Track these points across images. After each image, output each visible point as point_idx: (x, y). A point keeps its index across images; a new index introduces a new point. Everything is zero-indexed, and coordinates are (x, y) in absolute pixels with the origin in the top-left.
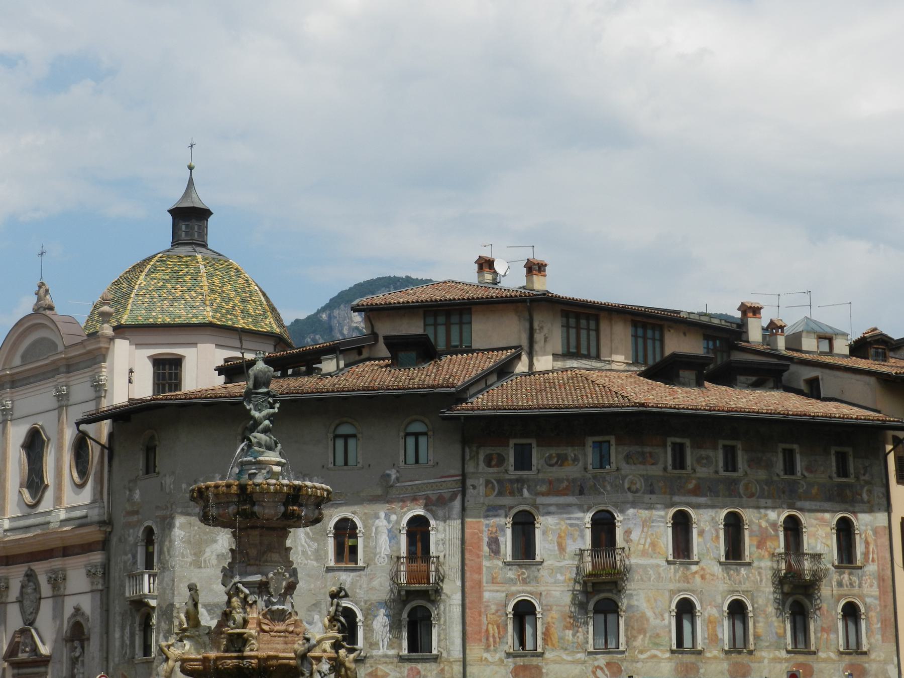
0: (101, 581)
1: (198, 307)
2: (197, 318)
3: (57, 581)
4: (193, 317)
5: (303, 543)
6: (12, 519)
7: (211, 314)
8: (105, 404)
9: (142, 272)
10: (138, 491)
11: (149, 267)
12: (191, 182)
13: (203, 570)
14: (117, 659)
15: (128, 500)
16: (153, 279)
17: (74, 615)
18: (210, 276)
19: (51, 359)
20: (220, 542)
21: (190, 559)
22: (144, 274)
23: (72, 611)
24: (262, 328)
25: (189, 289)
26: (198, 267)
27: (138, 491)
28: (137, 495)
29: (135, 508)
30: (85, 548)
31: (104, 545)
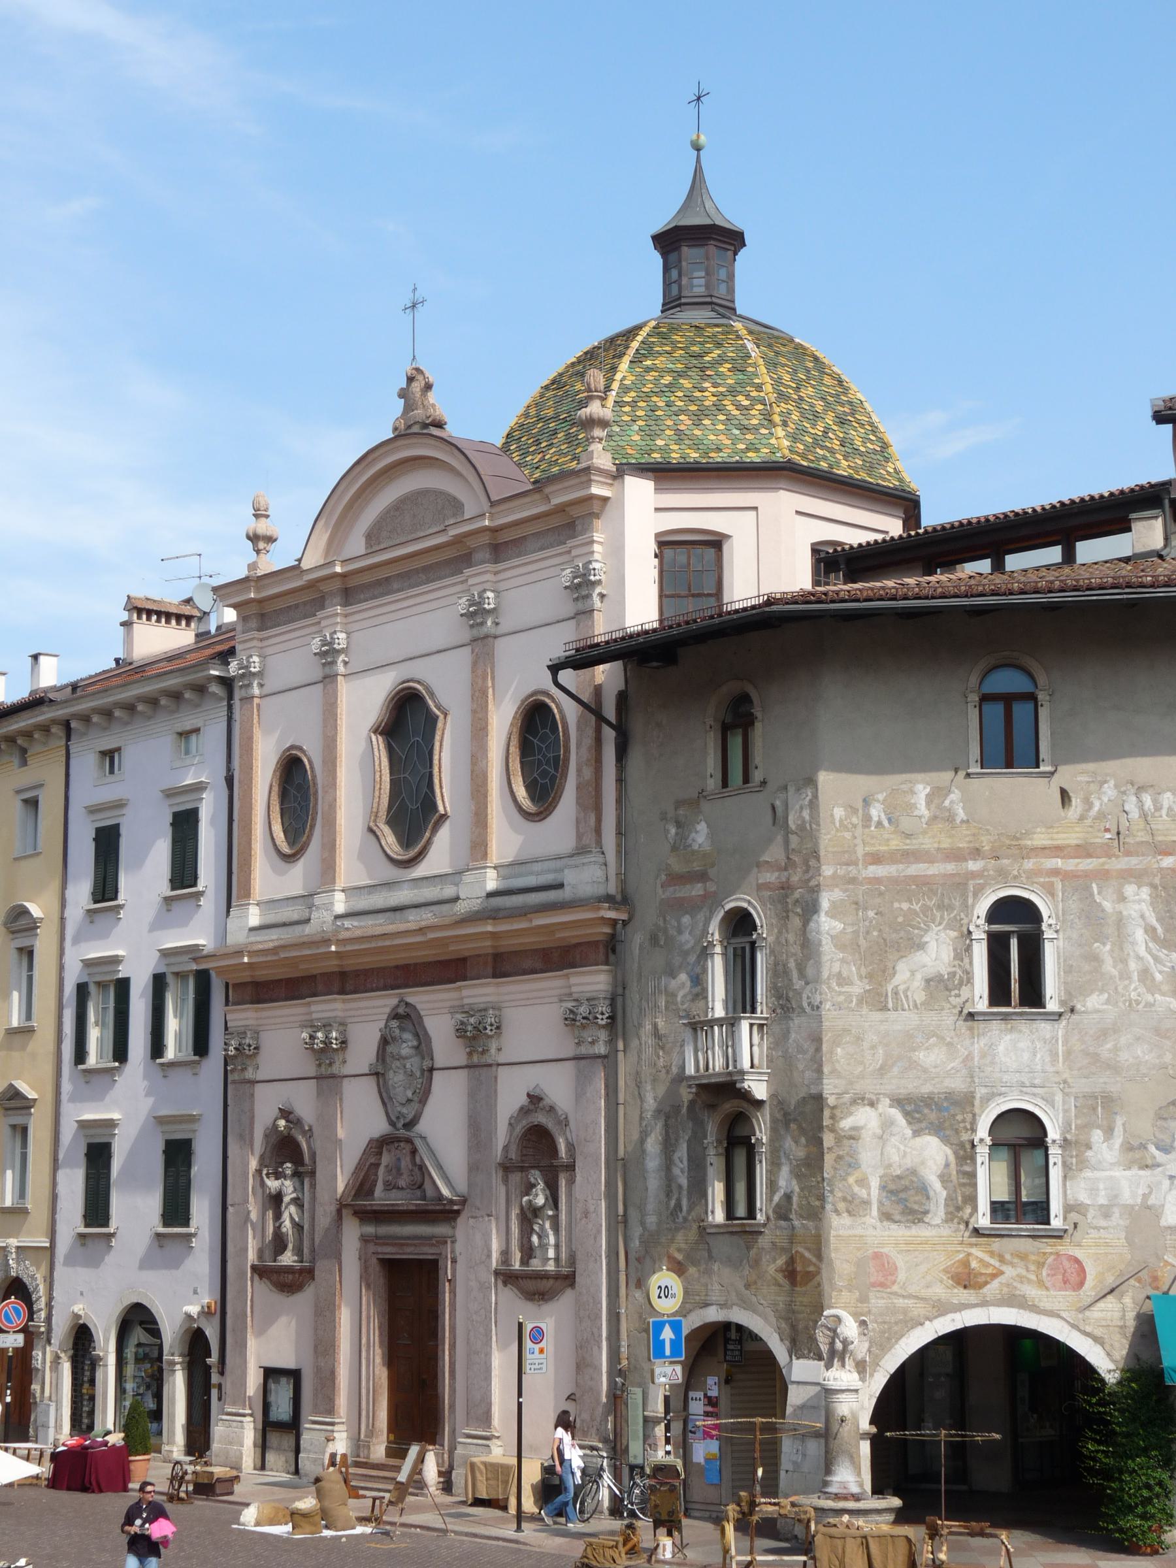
0: (603, 1035)
1: (756, 429)
2: (757, 450)
3: (476, 1035)
4: (748, 449)
5: (1142, 951)
6: (267, 905)
7: (786, 443)
8: (602, 628)
9: (621, 356)
10: (702, 827)
11: (635, 345)
12: (698, 172)
13: (892, 1015)
14: (651, 1220)
15: (674, 848)
16: (648, 370)
17: (524, 1111)
18: (772, 365)
19: (453, 532)
20: (932, 946)
21: (858, 988)
22: (626, 360)
23: (523, 1100)
24: (884, 479)
25: (733, 392)
26: (744, 346)
27: (702, 827)
28: (700, 836)
29: (696, 867)
30: (558, 957)
31: (610, 948)
